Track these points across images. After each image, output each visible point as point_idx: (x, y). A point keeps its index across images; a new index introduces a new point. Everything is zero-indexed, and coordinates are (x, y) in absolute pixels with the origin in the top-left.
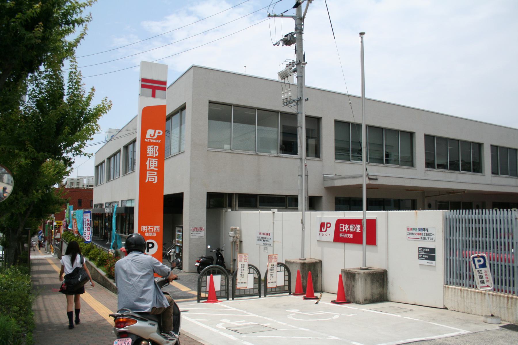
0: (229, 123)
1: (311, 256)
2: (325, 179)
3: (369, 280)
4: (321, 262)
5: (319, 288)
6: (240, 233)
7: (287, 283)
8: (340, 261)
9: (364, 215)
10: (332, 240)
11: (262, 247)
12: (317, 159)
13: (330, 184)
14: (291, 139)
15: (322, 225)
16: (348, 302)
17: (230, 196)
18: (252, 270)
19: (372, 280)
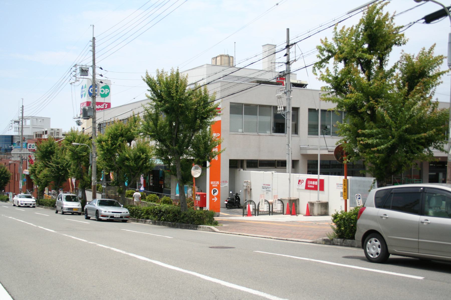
0: (241, 115)
1: (293, 197)
2: (301, 149)
3: (320, 206)
4: (298, 199)
5: (298, 212)
6: (250, 185)
7: (282, 209)
8: (306, 198)
9: (319, 177)
10: (304, 188)
11: (265, 192)
12: (296, 135)
13: (304, 152)
14: (280, 121)
15: (300, 181)
16: (311, 216)
17: (242, 161)
18: (266, 203)
19: (321, 206)
